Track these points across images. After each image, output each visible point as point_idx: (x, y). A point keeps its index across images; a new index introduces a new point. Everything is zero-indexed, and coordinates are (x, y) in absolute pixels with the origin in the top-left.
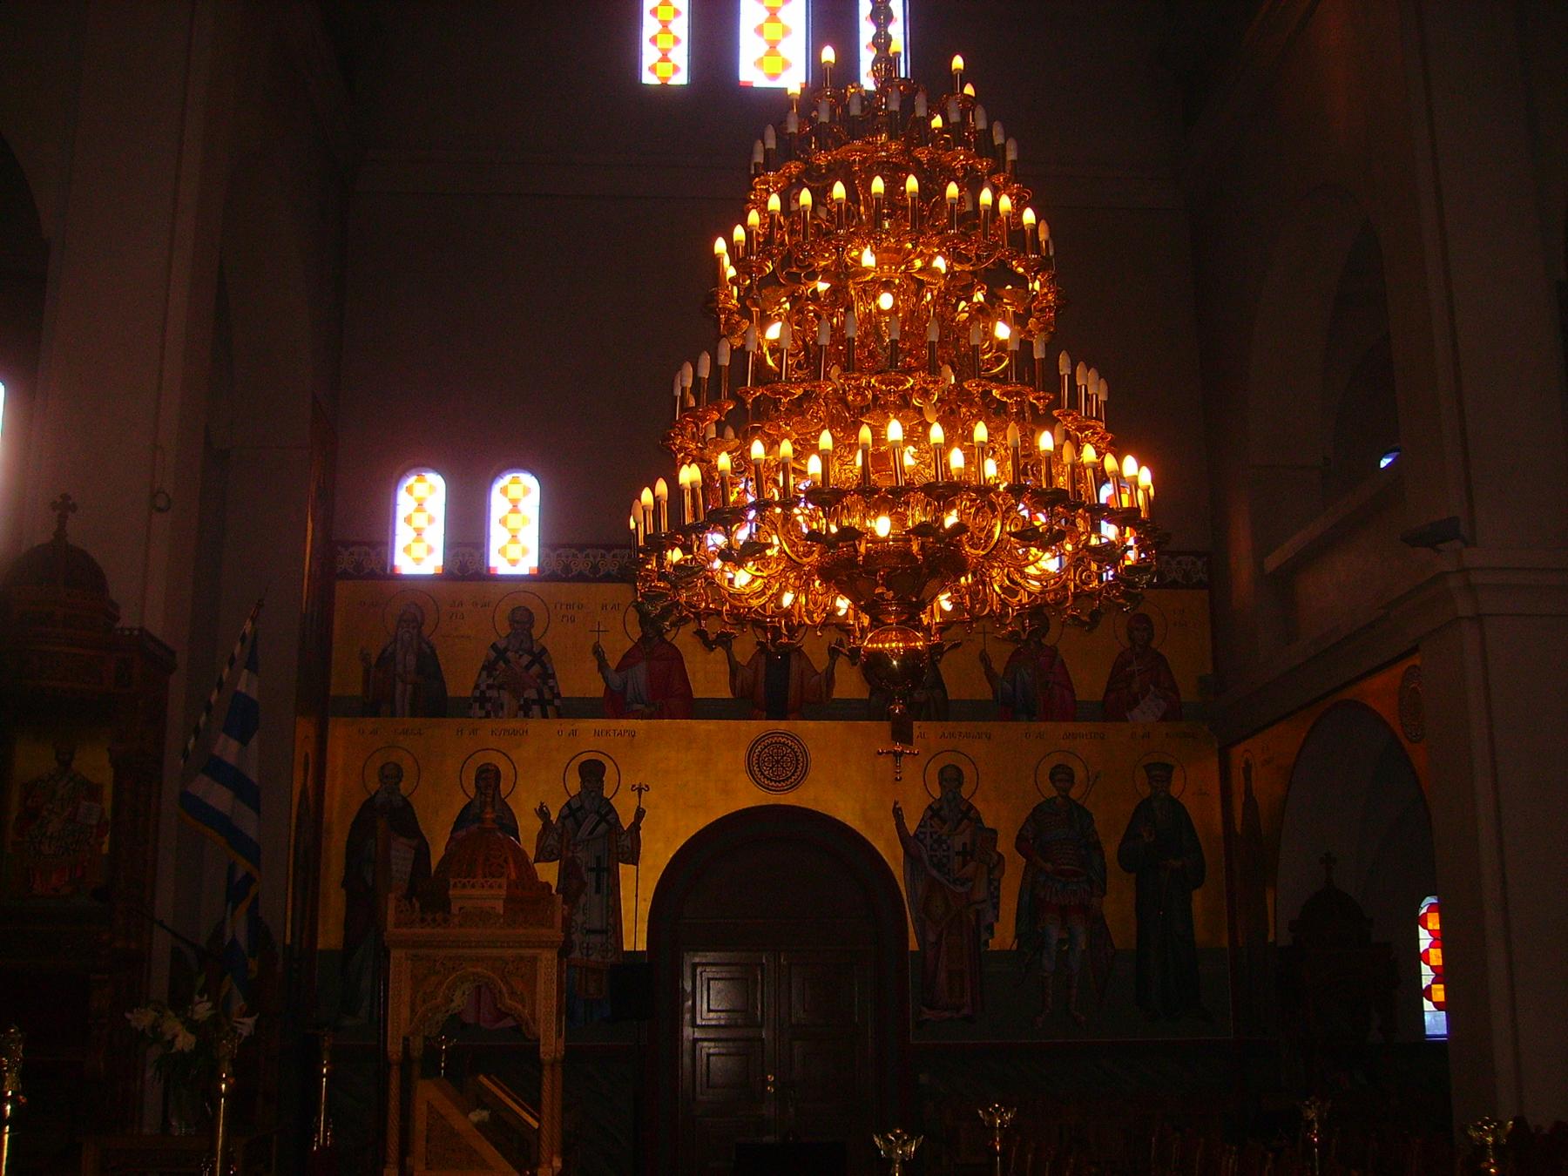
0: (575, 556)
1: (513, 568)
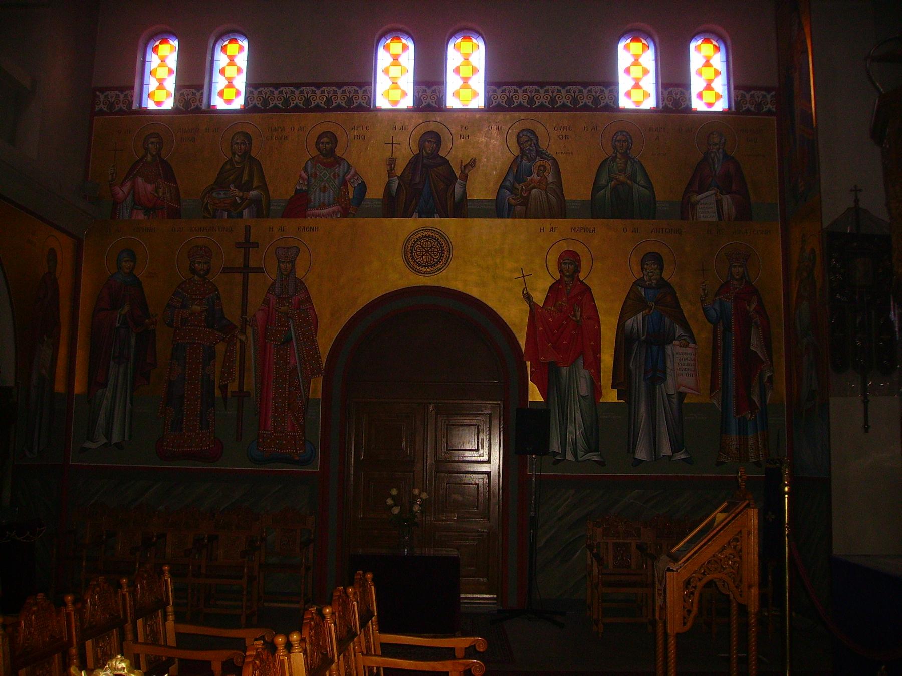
0: (516, 91)
1: (624, 94)
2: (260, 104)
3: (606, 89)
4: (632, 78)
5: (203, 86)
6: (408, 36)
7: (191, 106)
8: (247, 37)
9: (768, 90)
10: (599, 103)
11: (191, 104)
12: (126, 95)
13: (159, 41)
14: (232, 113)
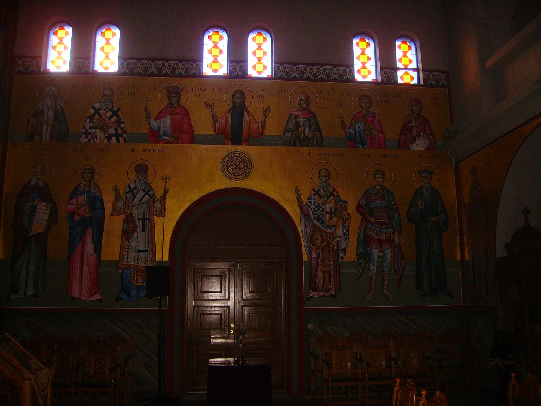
2: (183, 72)
3: (194, 63)
4: (403, 65)
5: (90, 57)
6: (266, 32)
7: (190, 73)
8: (118, 27)
9: (443, 72)
10: (317, 77)
11: (176, 71)
12: (241, 66)
13: (105, 29)
14: (262, 79)
